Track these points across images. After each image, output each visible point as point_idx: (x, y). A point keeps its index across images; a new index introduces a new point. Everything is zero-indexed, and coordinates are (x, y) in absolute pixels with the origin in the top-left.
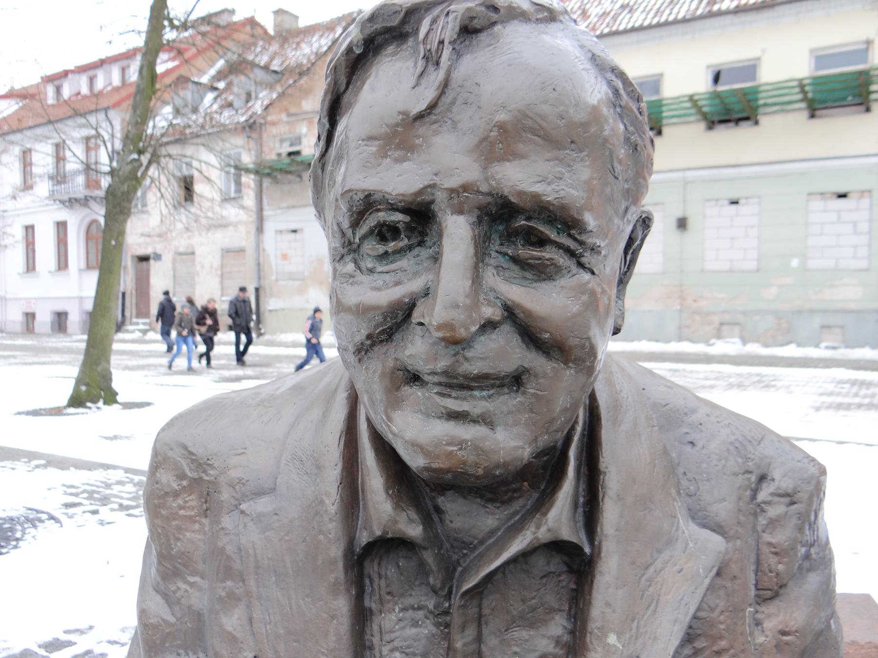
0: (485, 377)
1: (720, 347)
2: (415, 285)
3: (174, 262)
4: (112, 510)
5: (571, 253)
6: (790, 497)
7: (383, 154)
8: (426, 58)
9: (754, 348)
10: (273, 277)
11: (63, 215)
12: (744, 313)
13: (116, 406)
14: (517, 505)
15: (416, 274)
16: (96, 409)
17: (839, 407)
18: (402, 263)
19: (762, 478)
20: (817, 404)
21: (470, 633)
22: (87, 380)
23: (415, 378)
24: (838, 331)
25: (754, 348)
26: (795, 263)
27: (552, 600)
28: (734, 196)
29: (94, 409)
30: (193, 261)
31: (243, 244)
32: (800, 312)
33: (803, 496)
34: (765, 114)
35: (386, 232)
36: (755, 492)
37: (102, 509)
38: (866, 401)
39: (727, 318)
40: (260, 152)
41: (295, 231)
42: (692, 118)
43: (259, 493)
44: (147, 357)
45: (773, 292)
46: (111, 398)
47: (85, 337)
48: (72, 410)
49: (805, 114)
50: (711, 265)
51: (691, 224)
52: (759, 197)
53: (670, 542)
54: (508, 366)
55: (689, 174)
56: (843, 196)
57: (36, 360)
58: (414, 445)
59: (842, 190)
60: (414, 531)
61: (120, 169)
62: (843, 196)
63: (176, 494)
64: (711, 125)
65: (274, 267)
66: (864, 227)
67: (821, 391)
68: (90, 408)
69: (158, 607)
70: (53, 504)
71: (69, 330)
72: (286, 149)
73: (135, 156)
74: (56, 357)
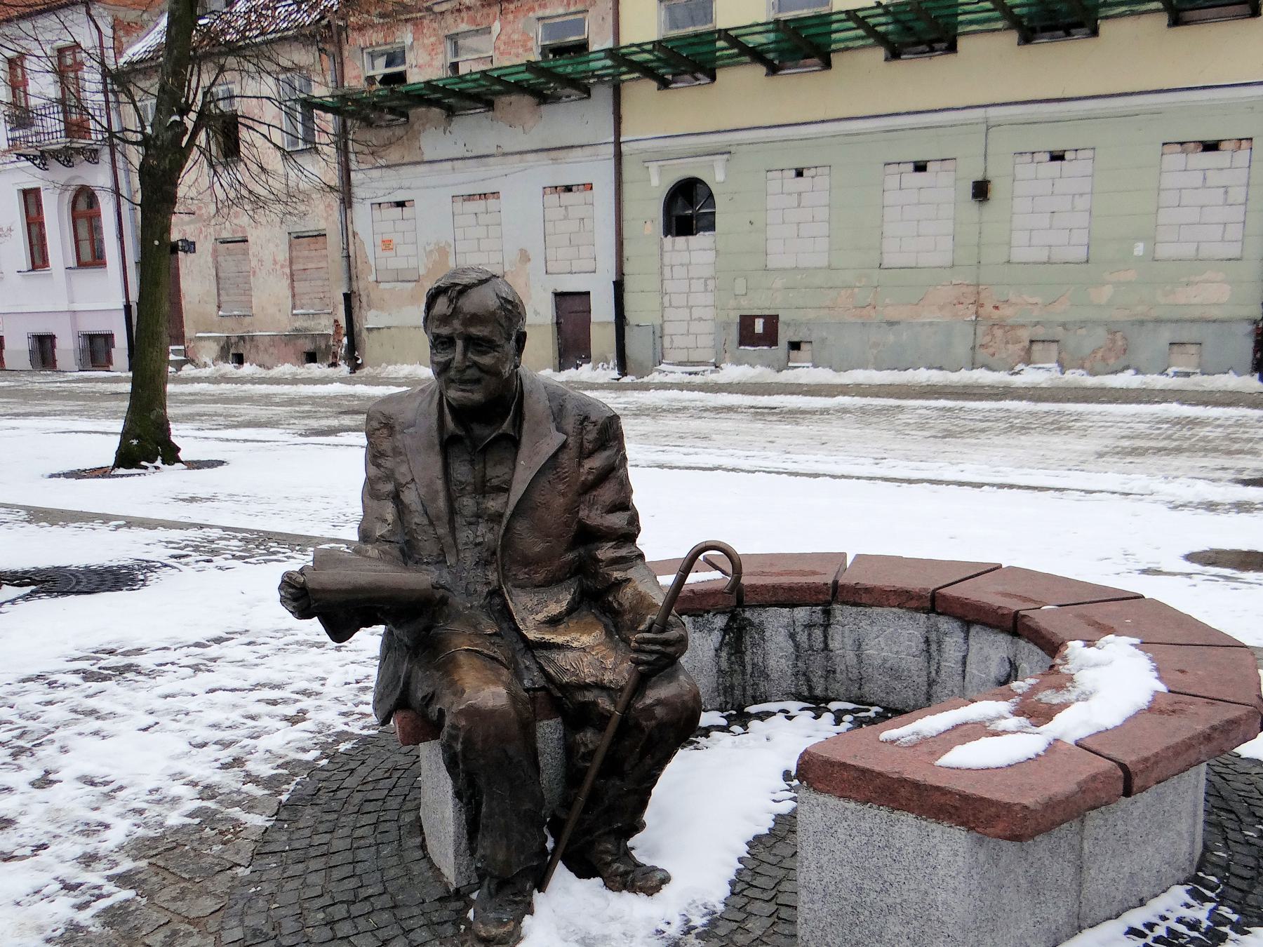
1: (1030, 377)
2: (451, 357)
3: (215, 254)
4: (226, 559)
9: (1076, 377)
10: (372, 278)
11: (30, 176)
12: (1064, 325)
13: (178, 465)
16: (154, 470)
21: (481, 465)
22: (138, 431)
23: (453, 381)
24: (1193, 349)
25: (1076, 377)
26: (1139, 249)
28: (1057, 147)
29: (151, 469)
30: (246, 253)
31: (322, 225)
32: (1142, 323)
34: (1107, 18)
35: (443, 343)
37: (214, 559)
39: (1040, 333)
40: (340, 79)
41: (401, 204)
42: (1000, 25)
43: (409, 427)
44: (193, 402)
46: (171, 455)
47: (131, 374)
48: (122, 471)
49: (1164, 18)
50: (1019, 254)
51: (995, 191)
52: (1094, 149)
55: (992, 112)
56: (1211, 146)
57: (28, 409)
58: (453, 399)
59: (1210, 137)
61: (157, 136)
62: (1211, 146)
64: (1027, 37)
65: (372, 262)
66: (1238, 194)
68: (146, 468)
69: (373, 470)
70: (159, 554)
71: (59, 365)
72: (380, 69)
73: (177, 118)
74: (58, 405)
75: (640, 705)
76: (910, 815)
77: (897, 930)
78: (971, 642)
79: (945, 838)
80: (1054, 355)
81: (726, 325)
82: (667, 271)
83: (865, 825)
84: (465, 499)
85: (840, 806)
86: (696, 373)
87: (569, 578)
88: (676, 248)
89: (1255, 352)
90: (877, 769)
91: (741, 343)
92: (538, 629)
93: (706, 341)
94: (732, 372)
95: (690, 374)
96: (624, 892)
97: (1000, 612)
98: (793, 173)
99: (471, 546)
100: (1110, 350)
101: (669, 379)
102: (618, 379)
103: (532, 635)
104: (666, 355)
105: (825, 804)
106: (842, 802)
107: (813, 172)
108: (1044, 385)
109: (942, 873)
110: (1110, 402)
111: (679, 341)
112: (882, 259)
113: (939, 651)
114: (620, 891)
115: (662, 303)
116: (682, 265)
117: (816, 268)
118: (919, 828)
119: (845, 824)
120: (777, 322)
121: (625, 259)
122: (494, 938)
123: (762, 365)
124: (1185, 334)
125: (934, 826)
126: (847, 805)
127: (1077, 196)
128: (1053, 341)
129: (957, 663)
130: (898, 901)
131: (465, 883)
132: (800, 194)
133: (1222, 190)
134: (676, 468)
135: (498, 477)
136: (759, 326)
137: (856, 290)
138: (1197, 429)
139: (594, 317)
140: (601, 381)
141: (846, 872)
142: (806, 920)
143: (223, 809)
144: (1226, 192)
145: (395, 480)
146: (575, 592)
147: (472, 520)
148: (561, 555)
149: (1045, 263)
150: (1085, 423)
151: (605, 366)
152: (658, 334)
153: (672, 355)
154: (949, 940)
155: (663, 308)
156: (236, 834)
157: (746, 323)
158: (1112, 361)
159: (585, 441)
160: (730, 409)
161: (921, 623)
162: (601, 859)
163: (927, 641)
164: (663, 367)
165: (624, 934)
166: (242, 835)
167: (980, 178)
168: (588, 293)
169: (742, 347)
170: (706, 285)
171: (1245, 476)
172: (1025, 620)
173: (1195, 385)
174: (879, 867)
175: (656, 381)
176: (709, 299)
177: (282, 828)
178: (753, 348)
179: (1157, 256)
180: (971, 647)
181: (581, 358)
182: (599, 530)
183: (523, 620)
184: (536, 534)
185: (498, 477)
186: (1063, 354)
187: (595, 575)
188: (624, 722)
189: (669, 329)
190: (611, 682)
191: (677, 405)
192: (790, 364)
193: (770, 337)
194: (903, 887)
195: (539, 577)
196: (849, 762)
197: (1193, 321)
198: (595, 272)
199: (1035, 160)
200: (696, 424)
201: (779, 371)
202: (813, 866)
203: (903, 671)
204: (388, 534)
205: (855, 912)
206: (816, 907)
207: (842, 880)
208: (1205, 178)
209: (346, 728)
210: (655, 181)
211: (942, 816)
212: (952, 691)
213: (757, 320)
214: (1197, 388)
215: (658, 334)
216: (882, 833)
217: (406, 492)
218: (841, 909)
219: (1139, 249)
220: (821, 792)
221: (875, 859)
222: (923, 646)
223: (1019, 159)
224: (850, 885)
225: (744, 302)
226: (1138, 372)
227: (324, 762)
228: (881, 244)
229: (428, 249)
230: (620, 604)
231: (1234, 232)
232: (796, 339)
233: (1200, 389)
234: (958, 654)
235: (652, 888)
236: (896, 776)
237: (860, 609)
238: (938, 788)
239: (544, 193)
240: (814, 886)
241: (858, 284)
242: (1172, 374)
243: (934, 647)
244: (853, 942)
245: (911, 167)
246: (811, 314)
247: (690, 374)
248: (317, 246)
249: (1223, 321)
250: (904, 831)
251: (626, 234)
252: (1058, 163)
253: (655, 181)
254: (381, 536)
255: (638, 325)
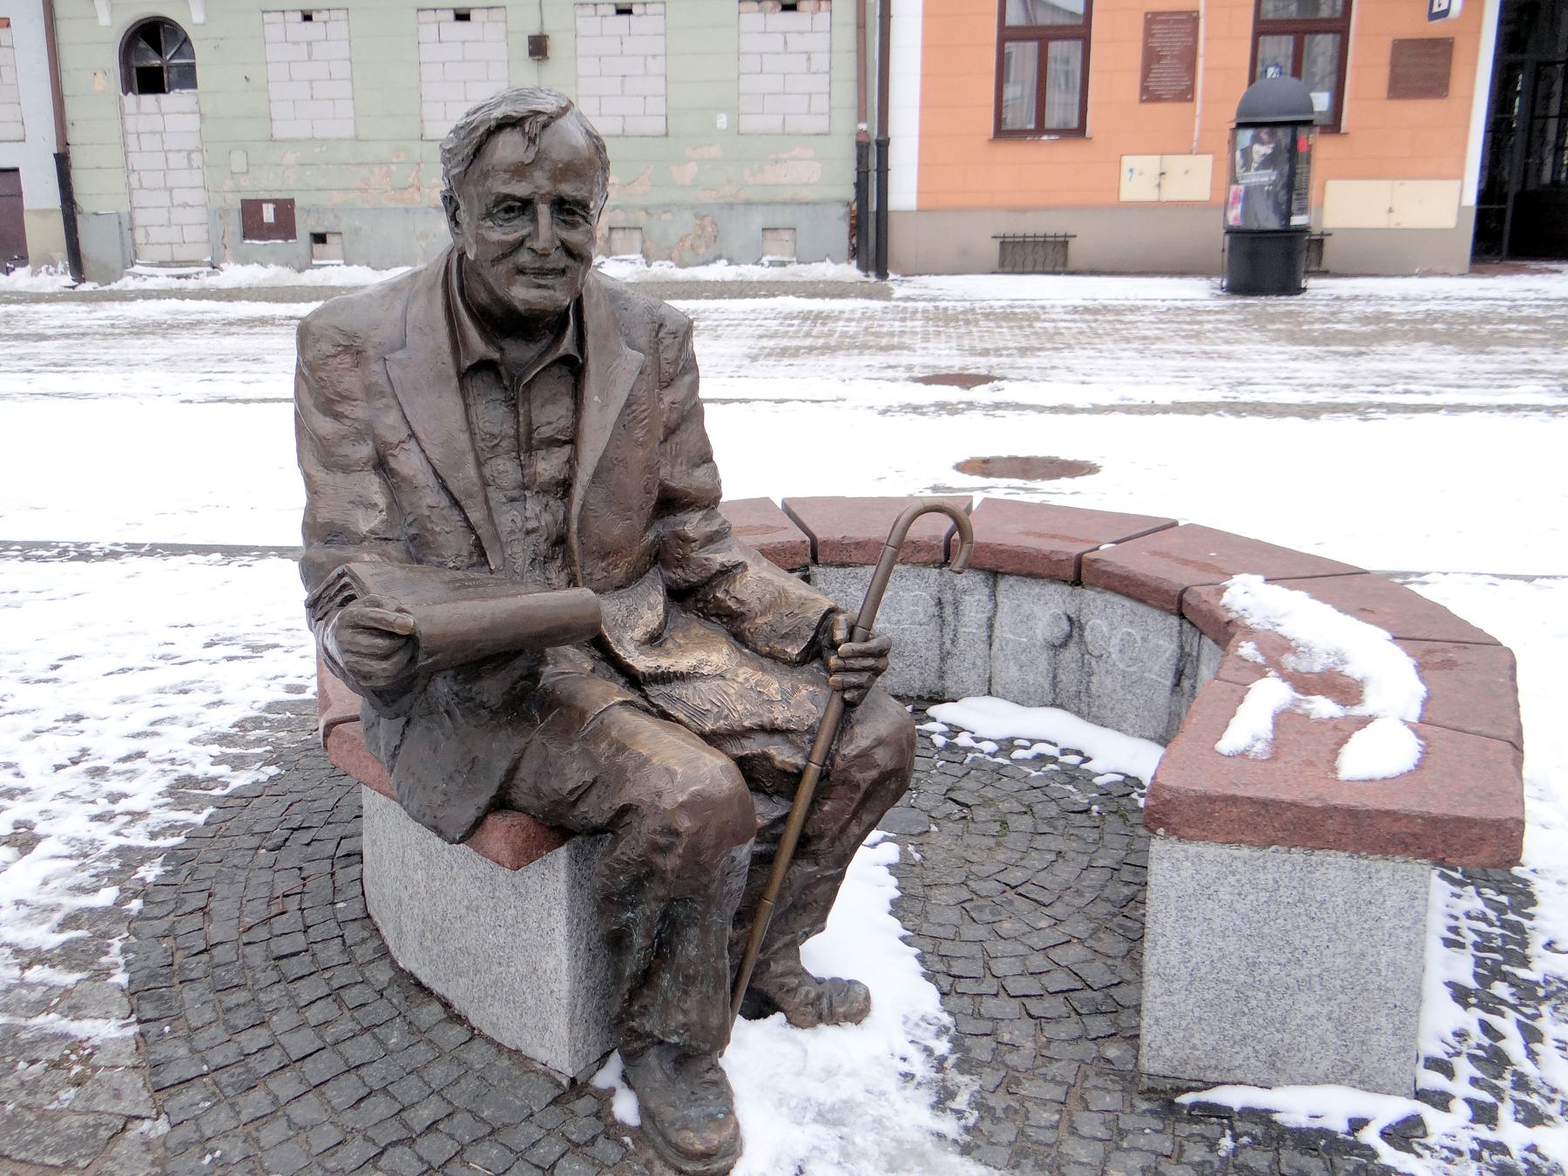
0: (554, 269)
2: (524, 232)
5: (584, 217)
6: (674, 334)
7: (512, 178)
8: (530, 139)
12: (646, 210)
14: (544, 342)
15: (523, 227)
17: (784, 352)
18: (516, 222)
19: (661, 326)
20: (754, 351)
23: (521, 271)
24: (787, 235)
26: (722, 121)
27: (563, 389)
32: (731, 206)
33: (681, 334)
36: (658, 333)
38: (820, 342)
45: (691, 170)
51: (555, 47)
53: (619, 356)
54: (562, 266)
60: (496, 356)
63: (334, 356)
66: (821, 61)
67: (760, 331)
75: (850, 750)
76: (1339, 853)
77: (1311, 1011)
78: (1000, 599)
79: (1397, 877)
80: (637, 244)
81: (222, 213)
82: (132, 140)
83: (1265, 878)
84: (500, 461)
85: (1225, 856)
86: (187, 277)
88: (142, 110)
89: (851, 237)
90: (1286, 797)
91: (245, 236)
93: (196, 234)
94: (234, 274)
95: (179, 277)
96: (821, 1027)
97: (1055, 558)
98: (299, 16)
99: (520, 536)
100: (699, 237)
101: (150, 284)
102: (73, 287)
104: (140, 255)
105: (1200, 856)
106: (1226, 852)
107: (325, 15)
108: (630, 280)
109: (1388, 925)
110: (715, 298)
111: (157, 234)
112: (423, 128)
113: (956, 614)
114: (813, 1025)
115: (129, 184)
116: (153, 133)
117: (339, 139)
118: (1356, 870)
119: (1232, 880)
120: (293, 208)
121: (68, 124)
122: (718, 1149)
123: (276, 264)
124: (782, 217)
125: (1380, 864)
126: (1236, 853)
127: (649, 58)
128: (635, 228)
129: (980, 627)
130: (1316, 971)
131: (582, 1066)
132: (309, 43)
133: (805, 56)
134: (238, 401)
135: (549, 423)
136: (268, 214)
137: (394, 168)
138: (830, 325)
139: (29, 203)
140: (49, 290)
141: (1231, 944)
142: (1157, 1020)
143: (22, 1022)
144: (809, 59)
145: (375, 438)
147: (516, 493)
149: (618, 136)
150: (708, 322)
151: (52, 269)
152: (126, 225)
153: (149, 254)
154: (1395, 1011)
155: (131, 191)
156: (84, 1060)
157: (250, 210)
158: (702, 250)
159: (663, 363)
160: (263, 321)
161: (931, 581)
162: (782, 986)
163: (940, 603)
164: (137, 269)
165: (868, 1091)
166: (98, 1059)
167: (536, 33)
168: (16, 170)
169: (248, 241)
170: (189, 160)
171: (917, 373)
172: (1096, 565)
173: (793, 275)
174: (1287, 931)
175: (131, 288)
176: (197, 179)
177: (162, 1034)
178: (262, 243)
179: (743, 129)
180: (1000, 606)
181: (12, 260)
182: (687, 495)
183: (619, 641)
184: (613, 508)
185: (549, 423)
186: (648, 243)
187: (683, 562)
188: (824, 776)
189: (141, 218)
190: (789, 721)
191: (185, 319)
192: (315, 262)
193: (285, 226)
194: (1326, 952)
195: (619, 573)
196: (1239, 793)
197: (784, 203)
198: (24, 140)
199: (600, 13)
200: (229, 343)
201: (300, 270)
202: (1174, 944)
203: (906, 644)
204: (383, 527)
205: (1241, 996)
206: (1175, 999)
207: (1224, 956)
208: (786, 42)
209: (122, 841)
210: (104, 19)
211: (1392, 850)
212: (974, 664)
213: (265, 206)
214: (797, 279)
215: (126, 225)
216: (1294, 883)
217: (402, 457)
218: (1218, 997)
219: (722, 121)
220: (1191, 839)
221: (1281, 921)
222: (935, 610)
223: (579, 12)
224: (1236, 961)
225: (245, 182)
226: (731, 262)
227: (136, 905)
228: (420, 109)
230: (741, 602)
231: (821, 103)
232: (320, 230)
233: (800, 279)
234: (979, 616)
235: (856, 1014)
236: (1317, 804)
237: (848, 570)
238: (1387, 813)
240: (1173, 971)
241: (395, 160)
242: (767, 264)
243: (949, 610)
244: (1238, 1038)
245: (451, 15)
246: (338, 198)
247: (179, 277)
249: (815, 204)
250: (1331, 876)
251: (67, 89)
252: (625, 18)
253: (104, 19)
254: (372, 532)
255: (97, 214)
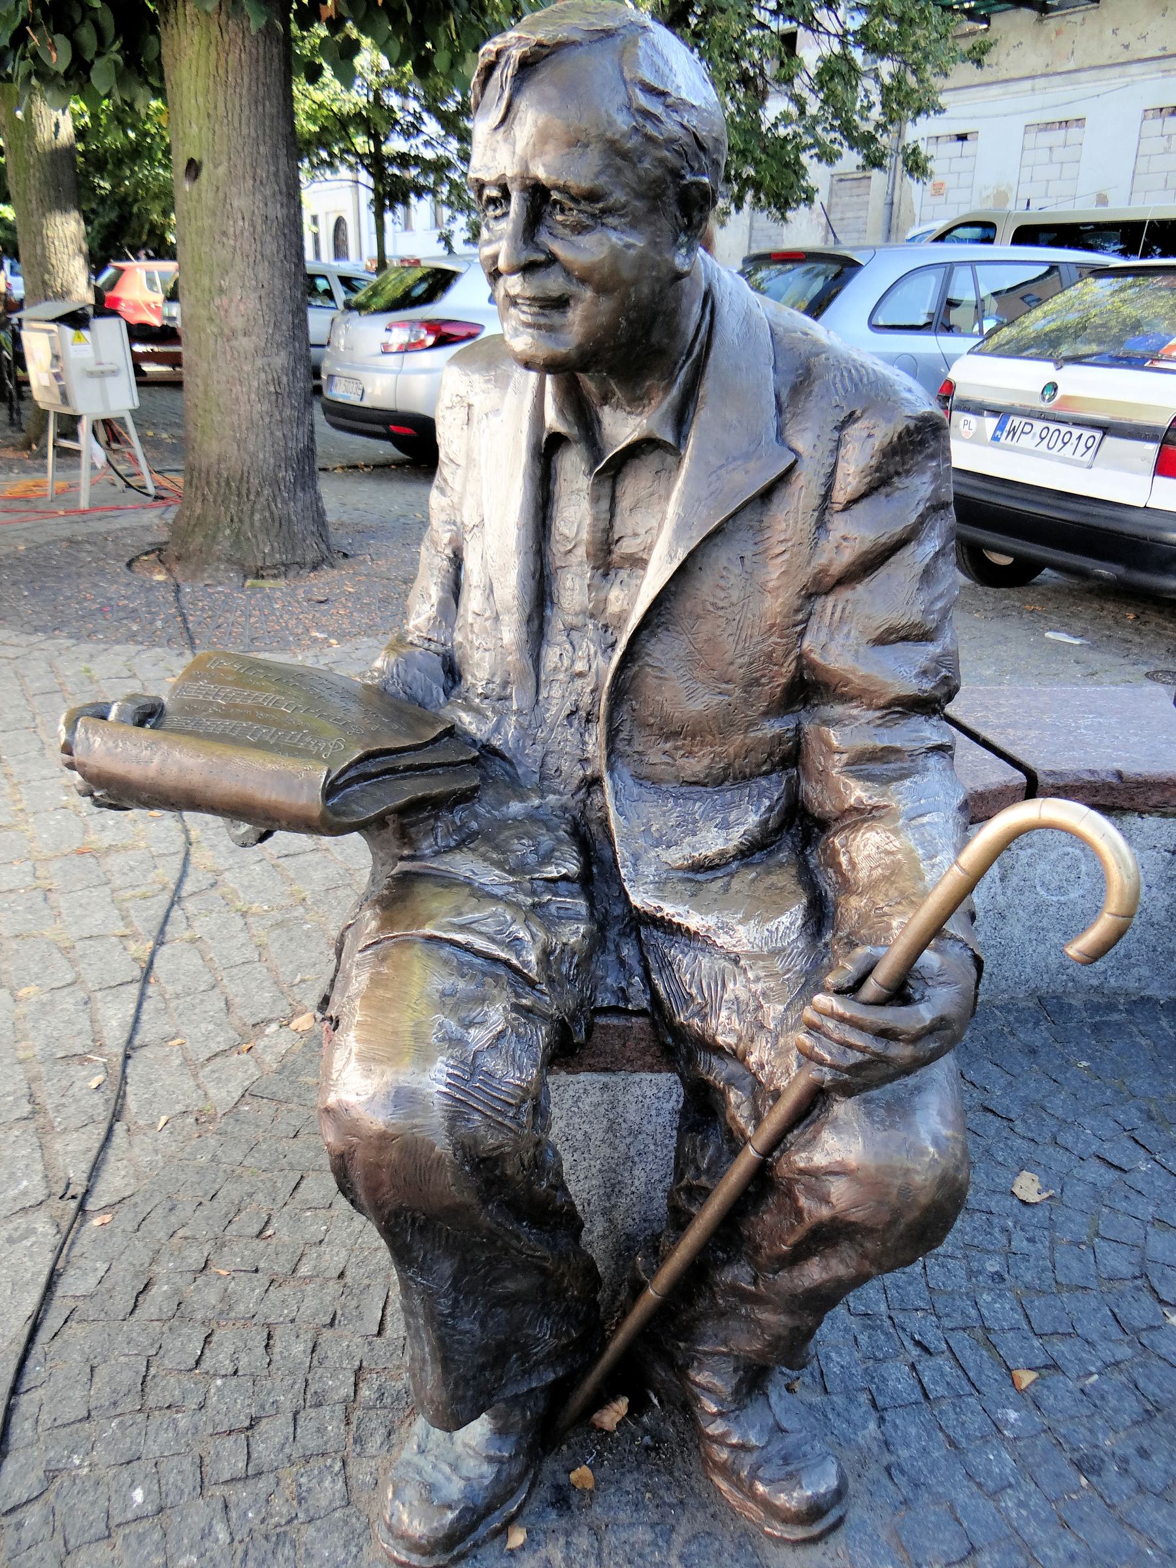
41: (962, 138)
87: (766, 774)
92: (661, 886)
103: (639, 899)
146: (770, 809)
148: (751, 724)
183: (636, 858)
195: (696, 766)
229: (984, 195)
239: (1145, 118)
248: (860, 191)
